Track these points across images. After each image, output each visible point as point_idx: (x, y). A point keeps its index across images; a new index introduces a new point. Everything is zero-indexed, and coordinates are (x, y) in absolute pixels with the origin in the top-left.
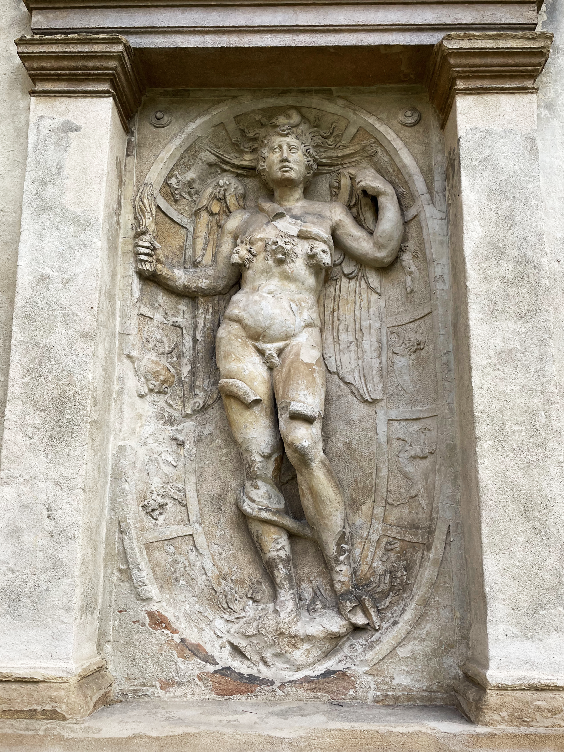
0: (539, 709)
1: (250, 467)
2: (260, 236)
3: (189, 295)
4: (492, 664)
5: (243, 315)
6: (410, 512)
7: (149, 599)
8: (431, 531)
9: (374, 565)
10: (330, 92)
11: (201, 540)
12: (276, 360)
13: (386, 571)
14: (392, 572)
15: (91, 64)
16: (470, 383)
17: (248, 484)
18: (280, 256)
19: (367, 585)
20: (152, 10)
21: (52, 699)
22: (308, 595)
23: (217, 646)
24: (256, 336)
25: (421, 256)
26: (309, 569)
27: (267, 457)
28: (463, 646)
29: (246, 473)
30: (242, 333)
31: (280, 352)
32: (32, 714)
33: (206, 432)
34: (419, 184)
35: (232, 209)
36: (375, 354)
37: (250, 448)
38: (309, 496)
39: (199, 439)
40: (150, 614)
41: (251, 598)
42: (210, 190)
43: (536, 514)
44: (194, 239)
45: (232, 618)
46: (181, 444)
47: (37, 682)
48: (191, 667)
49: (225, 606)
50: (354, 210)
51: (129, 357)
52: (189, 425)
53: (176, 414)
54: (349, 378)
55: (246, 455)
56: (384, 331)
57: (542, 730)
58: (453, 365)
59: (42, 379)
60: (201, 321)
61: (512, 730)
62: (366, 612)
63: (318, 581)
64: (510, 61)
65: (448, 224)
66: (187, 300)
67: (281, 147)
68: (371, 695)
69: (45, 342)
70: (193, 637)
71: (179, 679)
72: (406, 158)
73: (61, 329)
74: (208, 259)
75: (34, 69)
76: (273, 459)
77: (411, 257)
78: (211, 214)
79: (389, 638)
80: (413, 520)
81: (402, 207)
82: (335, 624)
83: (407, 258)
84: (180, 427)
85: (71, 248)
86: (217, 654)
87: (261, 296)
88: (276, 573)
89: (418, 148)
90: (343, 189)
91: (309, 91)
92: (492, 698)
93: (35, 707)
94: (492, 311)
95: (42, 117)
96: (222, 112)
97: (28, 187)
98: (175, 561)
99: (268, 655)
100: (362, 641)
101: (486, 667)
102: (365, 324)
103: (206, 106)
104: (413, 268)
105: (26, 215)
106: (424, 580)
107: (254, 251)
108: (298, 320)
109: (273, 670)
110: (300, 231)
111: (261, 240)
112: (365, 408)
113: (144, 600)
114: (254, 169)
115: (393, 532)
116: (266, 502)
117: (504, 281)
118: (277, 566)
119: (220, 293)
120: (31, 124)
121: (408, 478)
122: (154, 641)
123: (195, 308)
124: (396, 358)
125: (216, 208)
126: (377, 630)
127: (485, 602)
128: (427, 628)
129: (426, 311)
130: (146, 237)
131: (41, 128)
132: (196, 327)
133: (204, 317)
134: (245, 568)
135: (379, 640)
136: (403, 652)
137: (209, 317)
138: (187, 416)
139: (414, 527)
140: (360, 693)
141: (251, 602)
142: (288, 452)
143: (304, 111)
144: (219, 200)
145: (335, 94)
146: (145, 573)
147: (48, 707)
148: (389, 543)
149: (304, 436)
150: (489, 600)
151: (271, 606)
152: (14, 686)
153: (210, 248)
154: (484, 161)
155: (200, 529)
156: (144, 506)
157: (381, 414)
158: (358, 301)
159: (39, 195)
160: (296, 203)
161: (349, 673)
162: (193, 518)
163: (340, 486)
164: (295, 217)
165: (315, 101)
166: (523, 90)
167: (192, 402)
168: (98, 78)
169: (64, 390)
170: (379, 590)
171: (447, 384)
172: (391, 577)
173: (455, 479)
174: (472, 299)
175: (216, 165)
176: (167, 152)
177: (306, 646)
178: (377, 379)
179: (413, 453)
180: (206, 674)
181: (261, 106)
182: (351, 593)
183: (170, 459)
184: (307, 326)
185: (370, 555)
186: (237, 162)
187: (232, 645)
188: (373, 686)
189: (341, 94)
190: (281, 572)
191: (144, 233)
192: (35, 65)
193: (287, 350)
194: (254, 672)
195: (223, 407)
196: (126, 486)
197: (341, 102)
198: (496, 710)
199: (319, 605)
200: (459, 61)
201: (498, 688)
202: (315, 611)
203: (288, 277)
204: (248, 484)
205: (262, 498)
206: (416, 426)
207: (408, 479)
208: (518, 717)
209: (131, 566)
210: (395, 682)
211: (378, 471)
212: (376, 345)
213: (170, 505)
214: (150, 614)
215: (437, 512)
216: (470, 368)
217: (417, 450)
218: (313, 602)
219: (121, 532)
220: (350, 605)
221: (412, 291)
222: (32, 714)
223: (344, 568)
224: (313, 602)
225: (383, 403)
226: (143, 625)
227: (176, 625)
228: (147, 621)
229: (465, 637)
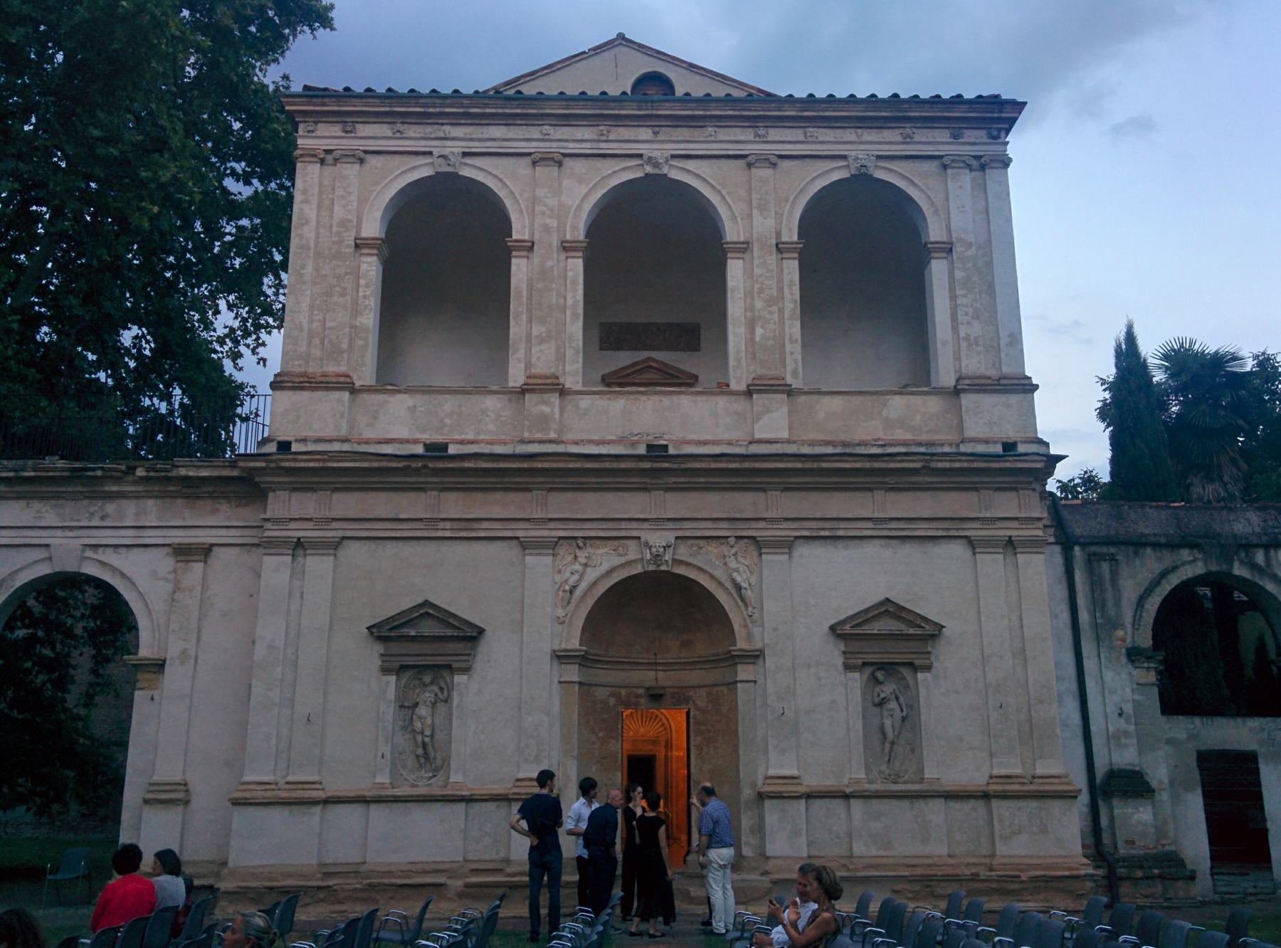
24: (420, 718)
205: (420, 751)
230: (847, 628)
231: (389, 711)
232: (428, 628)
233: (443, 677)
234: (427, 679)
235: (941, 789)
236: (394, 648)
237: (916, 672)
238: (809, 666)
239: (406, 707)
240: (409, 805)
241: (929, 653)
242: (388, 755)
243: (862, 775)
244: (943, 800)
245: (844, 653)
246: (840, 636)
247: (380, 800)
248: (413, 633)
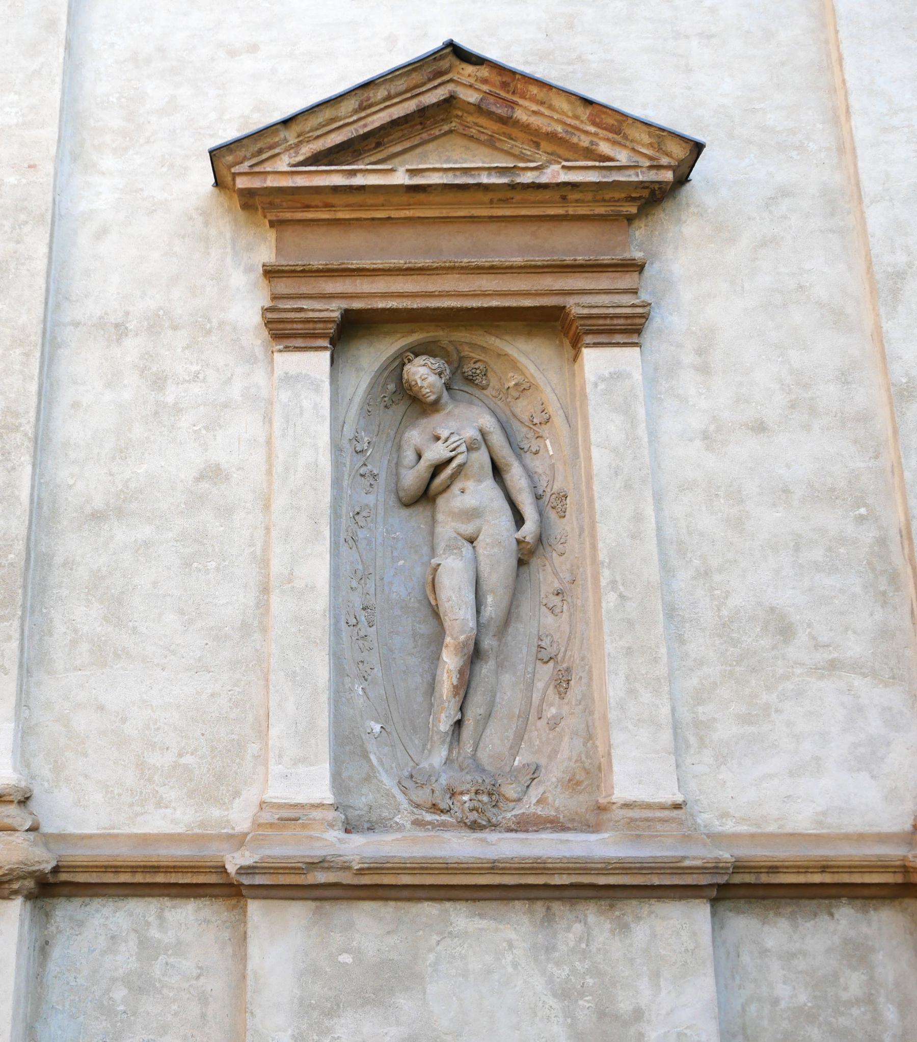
230: (282, 170)
232: (326, 865)
235: (698, 854)
237: (576, 344)
238: (120, 330)
240: (630, 908)
241: (638, 267)
243: (314, 786)
244: (700, 914)
245: (271, 273)
246: (250, 201)
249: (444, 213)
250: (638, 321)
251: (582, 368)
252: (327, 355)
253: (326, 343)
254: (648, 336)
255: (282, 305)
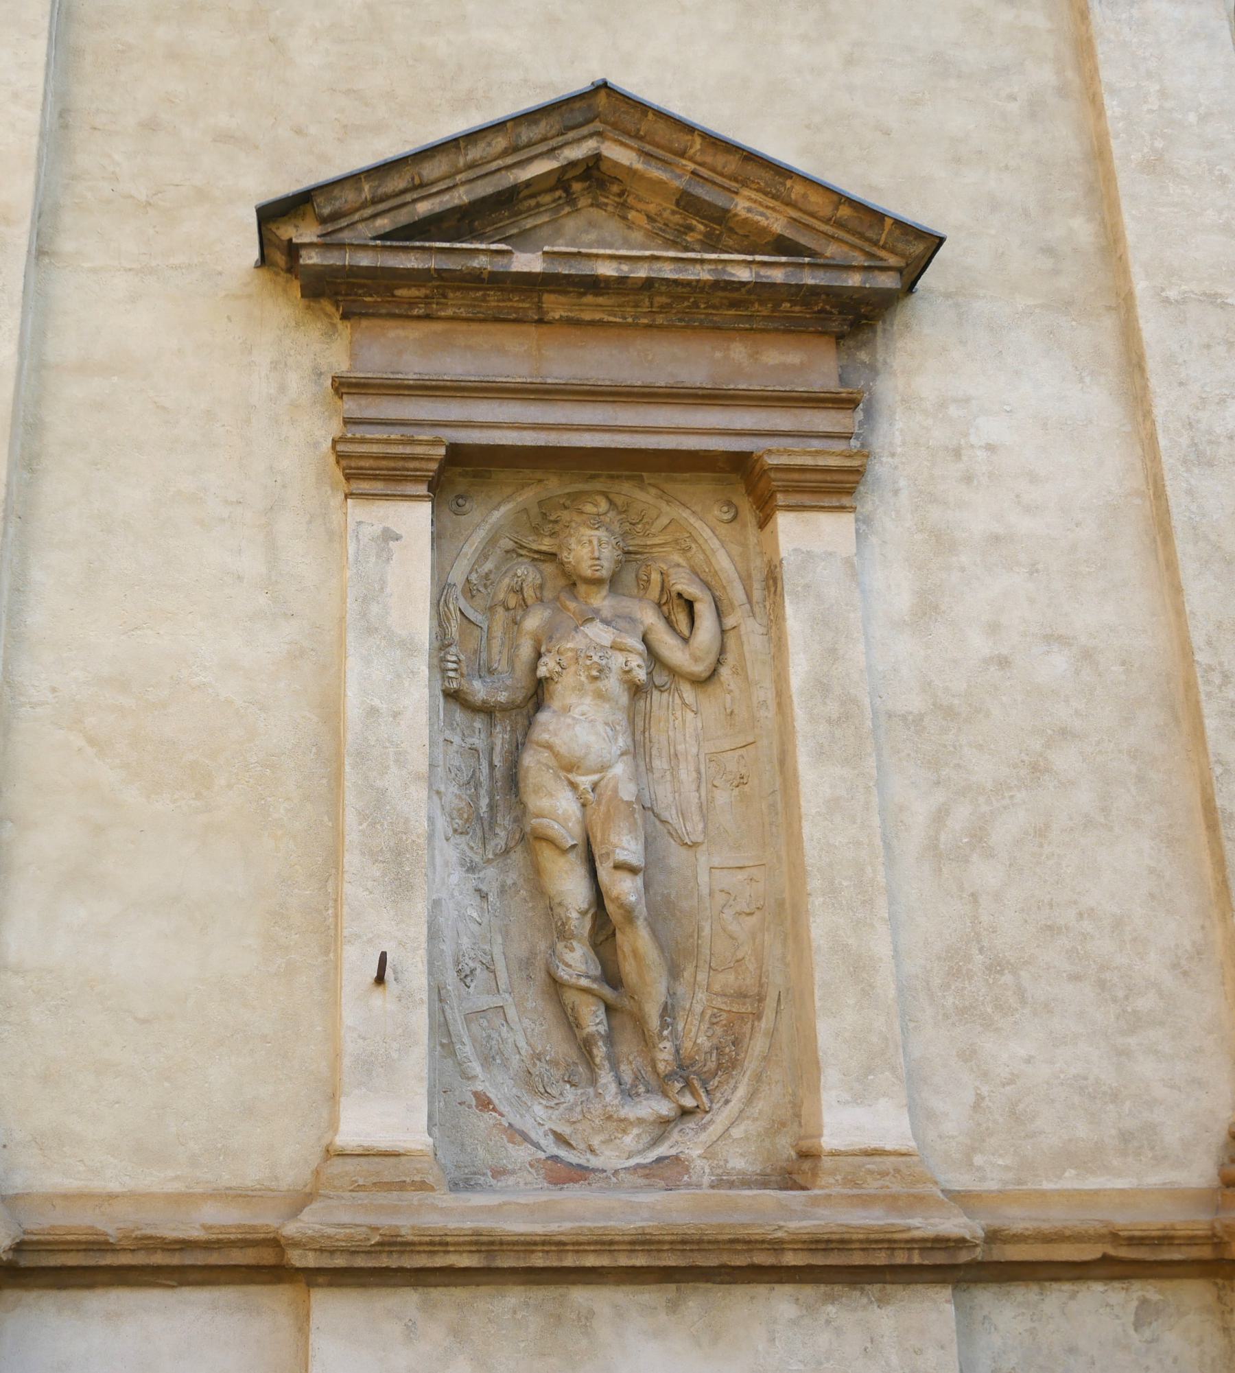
0: (871, 1172)
1: (563, 924)
2: (570, 645)
3: (487, 711)
4: (826, 1132)
5: (557, 741)
6: (737, 978)
7: (475, 1077)
8: (761, 999)
9: (699, 1041)
10: (641, 479)
11: (512, 1013)
12: (590, 796)
13: (712, 1048)
14: (719, 1049)
15: (412, 465)
16: (800, 833)
17: (560, 946)
18: (595, 673)
19: (692, 1065)
20: (469, 401)
21: (419, 1171)
22: (628, 1078)
23: (541, 1133)
24: (568, 766)
25: (740, 671)
26: (628, 1046)
27: (583, 913)
28: (796, 1124)
29: (562, 933)
30: (553, 762)
31: (594, 787)
32: (402, 1186)
33: (509, 882)
34: (738, 594)
35: (529, 602)
36: (694, 787)
37: (565, 902)
38: (631, 960)
39: (503, 890)
40: (476, 1094)
41: (569, 1082)
42: (507, 581)
43: (865, 975)
44: (489, 640)
45: (552, 1103)
46: (484, 896)
47: (398, 1155)
48: (521, 1154)
49: (542, 1090)
50: (665, 608)
51: (438, 793)
52: (490, 872)
53: (477, 859)
54: (665, 815)
55: (558, 910)
56: (702, 757)
57: (872, 1191)
58: (780, 806)
59: (378, 826)
60: (498, 742)
61: (845, 1191)
62: (694, 1094)
63: (639, 1062)
64: (829, 478)
65: (770, 639)
66: (482, 716)
67: (590, 542)
68: (706, 1180)
69: (379, 783)
70: (518, 1123)
71: (510, 1167)
72: (723, 563)
73: (394, 769)
74: (502, 666)
75: (351, 468)
76: (590, 915)
77: (730, 672)
78: (507, 609)
79: (721, 1118)
80: (740, 987)
81: (720, 614)
82: (665, 1108)
83: (725, 672)
84: (481, 875)
85: (399, 676)
86: (543, 1142)
87: (574, 718)
88: (595, 1051)
89: (736, 550)
90: (652, 585)
91: (618, 477)
92: (827, 1162)
93: (403, 1178)
94: (821, 754)
95: (360, 523)
96: (528, 496)
97: (352, 606)
98: (489, 1036)
99: (596, 1141)
100: (692, 1125)
101: (820, 1135)
102: (681, 748)
103: (509, 490)
104: (732, 687)
105: (350, 637)
106: (756, 1053)
107: (564, 663)
108: (614, 748)
109: (602, 1158)
110: (614, 642)
111: (571, 650)
112: (683, 852)
113: (469, 1079)
114: (554, 555)
115: (719, 1002)
116: (583, 968)
117: (829, 721)
118: (596, 1044)
119: (518, 707)
120: (350, 530)
121: (731, 937)
122: (482, 1124)
123: (492, 725)
124: (717, 793)
125: (512, 602)
126: (707, 1112)
127: (819, 1069)
128: (760, 1106)
129: (751, 740)
130: (453, 650)
131: (360, 537)
132: (492, 749)
133: (501, 738)
134: (558, 1046)
135: (711, 1122)
136: (737, 1132)
137: (507, 736)
138: (489, 861)
139: (741, 995)
140: (694, 1178)
141: (568, 1086)
142: (610, 907)
143: (611, 496)
144: (516, 592)
145: (647, 481)
146: (467, 1050)
147: (417, 1178)
148: (714, 1015)
149: (625, 888)
150: (822, 1065)
151: (591, 1090)
152: (377, 1159)
153: (505, 652)
154: (807, 587)
155: (510, 1000)
156: (459, 971)
157: (703, 859)
158: (671, 718)
159: (364, 615)
160: (601, 601)
161: (682, 1156)
162: (502, 986)
163: (661, 948)
164: (606, 622)
165: (626, 487)
166: (842, 508)
167: (493, 843)
168: (416, 480)
169: (401, 839)
170: (705, 1069)
171: (774, 829)
172: (718, 1054)
173: (785, 940)
174: (799, 740)
175: (513, 550)
176: (471, 546)
177: (635, 1131)
178: (696, 818)
179: (738, 909)
180: (538, 1160)
181: (567, 491)
182: (676, 1073)
183: (475, 915)
184: (622, 754)
185: (694, 1030)
186: (535, 547)
187: (554, 1133)
188: (707, 1170)
189: (652, 481)
190: (600, 1051)
191: (450, 645)
192: (353, 464)
193: (603, 783)
194: (583, 1162)
195: (531, 853)
196: (444, 947)
197: (653, 491)
198: (832, 1173)
199: (642, 1089)
200: (779, 475)
201: (834, 1154)
202: (638, 1095)
203: (600, 696)
204: (560, 946)
205: (577, 961)
206: (741, 876)
207: (733, 939)
208: (851, 1181)
209: (454, 1040)
210: (730, 1165)
211: (700, 929)
212: (694, 775)
213: (478, 970)
214: (476, 1094)
215: (767, 977)
216: (800, 818)
217: (742, 905)
218: (635, 1086)
219: (440, 1000)
220: (678, 1085)
221: (732, 712)
222: (402, 1186)
223: (668, 1044)
224: (635, 1086)
225: (704, 847)
226: (470, 1107)
227: (501, 1108)
228: (474, 1103)
229: (797, 1116)
231: (395, 697)
232: (606, 245)
233: (684, 543)
234: (590, 547)
236: (402, 349)
239: (497, 712)
242: (413, 971)
247: (386, 1267)
248: (528, 262)
249: (401, 244)
250: (852, 478)
251: (774, 533)
252: (425, 508)
253: (422, 489)
254: (870, 501)
255: (360, 432)
